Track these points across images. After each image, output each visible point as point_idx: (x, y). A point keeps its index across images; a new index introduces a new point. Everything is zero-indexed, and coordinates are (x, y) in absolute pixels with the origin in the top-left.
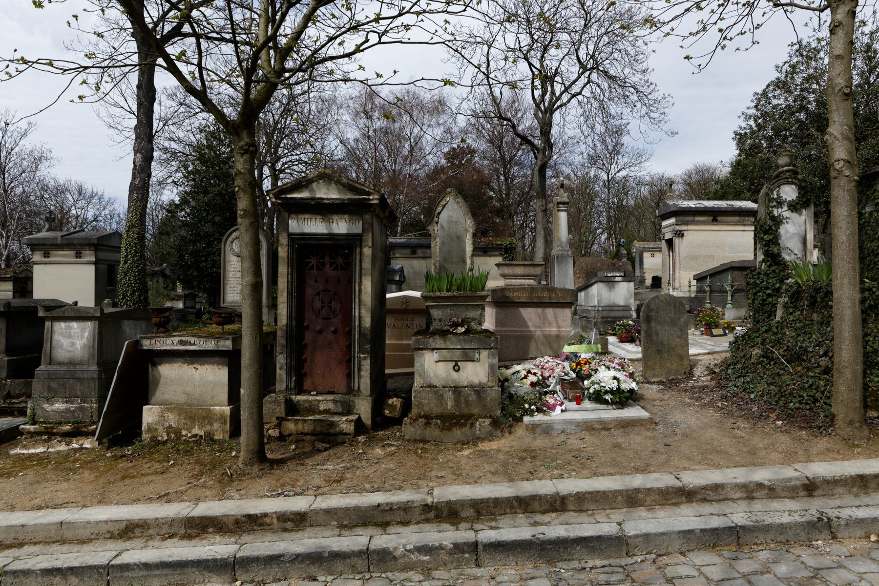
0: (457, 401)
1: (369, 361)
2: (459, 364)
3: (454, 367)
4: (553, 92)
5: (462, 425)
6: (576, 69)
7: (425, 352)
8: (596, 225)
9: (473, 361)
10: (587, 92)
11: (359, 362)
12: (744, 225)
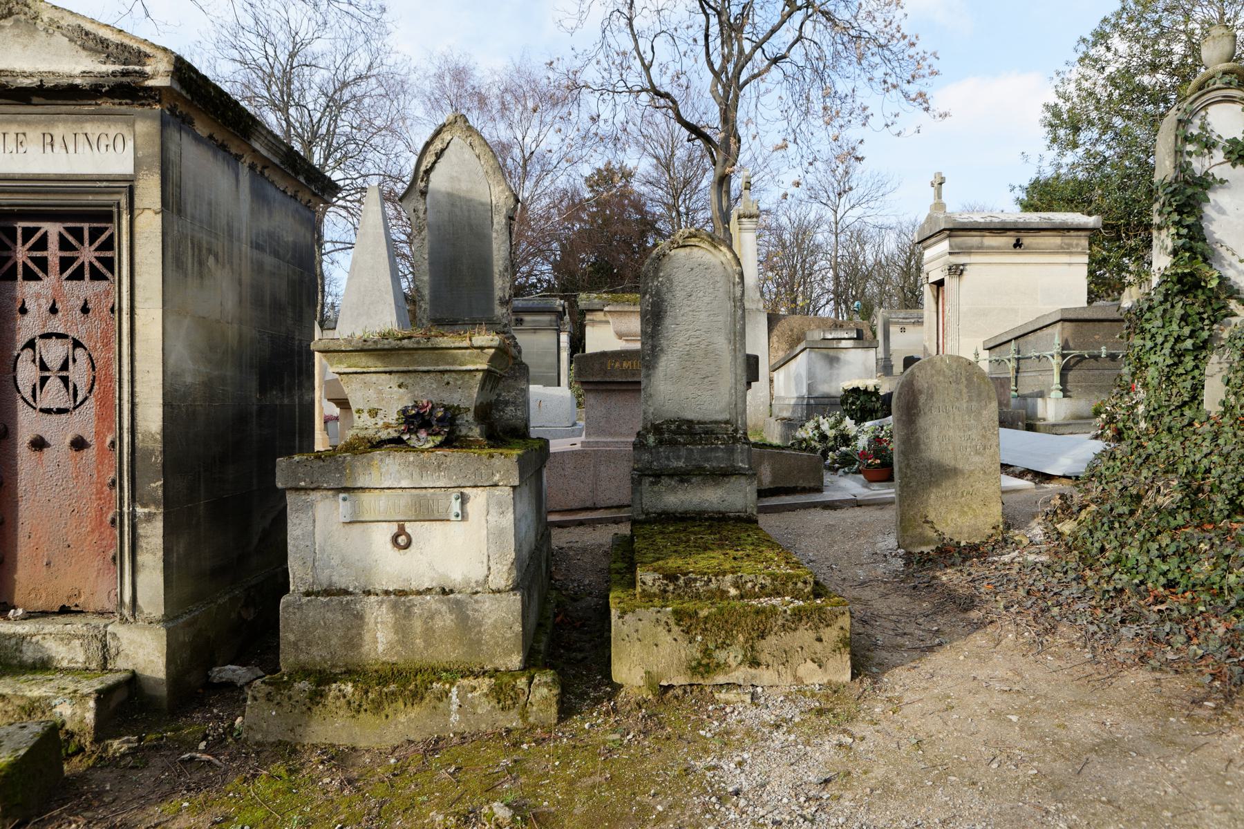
0: (403, 631)
2: (409, 528)
3: (395, 539)
4: (741, 51)
5: (417, 697)
8: (818, 291)
10: (797, 54)
12: (1071, 253)
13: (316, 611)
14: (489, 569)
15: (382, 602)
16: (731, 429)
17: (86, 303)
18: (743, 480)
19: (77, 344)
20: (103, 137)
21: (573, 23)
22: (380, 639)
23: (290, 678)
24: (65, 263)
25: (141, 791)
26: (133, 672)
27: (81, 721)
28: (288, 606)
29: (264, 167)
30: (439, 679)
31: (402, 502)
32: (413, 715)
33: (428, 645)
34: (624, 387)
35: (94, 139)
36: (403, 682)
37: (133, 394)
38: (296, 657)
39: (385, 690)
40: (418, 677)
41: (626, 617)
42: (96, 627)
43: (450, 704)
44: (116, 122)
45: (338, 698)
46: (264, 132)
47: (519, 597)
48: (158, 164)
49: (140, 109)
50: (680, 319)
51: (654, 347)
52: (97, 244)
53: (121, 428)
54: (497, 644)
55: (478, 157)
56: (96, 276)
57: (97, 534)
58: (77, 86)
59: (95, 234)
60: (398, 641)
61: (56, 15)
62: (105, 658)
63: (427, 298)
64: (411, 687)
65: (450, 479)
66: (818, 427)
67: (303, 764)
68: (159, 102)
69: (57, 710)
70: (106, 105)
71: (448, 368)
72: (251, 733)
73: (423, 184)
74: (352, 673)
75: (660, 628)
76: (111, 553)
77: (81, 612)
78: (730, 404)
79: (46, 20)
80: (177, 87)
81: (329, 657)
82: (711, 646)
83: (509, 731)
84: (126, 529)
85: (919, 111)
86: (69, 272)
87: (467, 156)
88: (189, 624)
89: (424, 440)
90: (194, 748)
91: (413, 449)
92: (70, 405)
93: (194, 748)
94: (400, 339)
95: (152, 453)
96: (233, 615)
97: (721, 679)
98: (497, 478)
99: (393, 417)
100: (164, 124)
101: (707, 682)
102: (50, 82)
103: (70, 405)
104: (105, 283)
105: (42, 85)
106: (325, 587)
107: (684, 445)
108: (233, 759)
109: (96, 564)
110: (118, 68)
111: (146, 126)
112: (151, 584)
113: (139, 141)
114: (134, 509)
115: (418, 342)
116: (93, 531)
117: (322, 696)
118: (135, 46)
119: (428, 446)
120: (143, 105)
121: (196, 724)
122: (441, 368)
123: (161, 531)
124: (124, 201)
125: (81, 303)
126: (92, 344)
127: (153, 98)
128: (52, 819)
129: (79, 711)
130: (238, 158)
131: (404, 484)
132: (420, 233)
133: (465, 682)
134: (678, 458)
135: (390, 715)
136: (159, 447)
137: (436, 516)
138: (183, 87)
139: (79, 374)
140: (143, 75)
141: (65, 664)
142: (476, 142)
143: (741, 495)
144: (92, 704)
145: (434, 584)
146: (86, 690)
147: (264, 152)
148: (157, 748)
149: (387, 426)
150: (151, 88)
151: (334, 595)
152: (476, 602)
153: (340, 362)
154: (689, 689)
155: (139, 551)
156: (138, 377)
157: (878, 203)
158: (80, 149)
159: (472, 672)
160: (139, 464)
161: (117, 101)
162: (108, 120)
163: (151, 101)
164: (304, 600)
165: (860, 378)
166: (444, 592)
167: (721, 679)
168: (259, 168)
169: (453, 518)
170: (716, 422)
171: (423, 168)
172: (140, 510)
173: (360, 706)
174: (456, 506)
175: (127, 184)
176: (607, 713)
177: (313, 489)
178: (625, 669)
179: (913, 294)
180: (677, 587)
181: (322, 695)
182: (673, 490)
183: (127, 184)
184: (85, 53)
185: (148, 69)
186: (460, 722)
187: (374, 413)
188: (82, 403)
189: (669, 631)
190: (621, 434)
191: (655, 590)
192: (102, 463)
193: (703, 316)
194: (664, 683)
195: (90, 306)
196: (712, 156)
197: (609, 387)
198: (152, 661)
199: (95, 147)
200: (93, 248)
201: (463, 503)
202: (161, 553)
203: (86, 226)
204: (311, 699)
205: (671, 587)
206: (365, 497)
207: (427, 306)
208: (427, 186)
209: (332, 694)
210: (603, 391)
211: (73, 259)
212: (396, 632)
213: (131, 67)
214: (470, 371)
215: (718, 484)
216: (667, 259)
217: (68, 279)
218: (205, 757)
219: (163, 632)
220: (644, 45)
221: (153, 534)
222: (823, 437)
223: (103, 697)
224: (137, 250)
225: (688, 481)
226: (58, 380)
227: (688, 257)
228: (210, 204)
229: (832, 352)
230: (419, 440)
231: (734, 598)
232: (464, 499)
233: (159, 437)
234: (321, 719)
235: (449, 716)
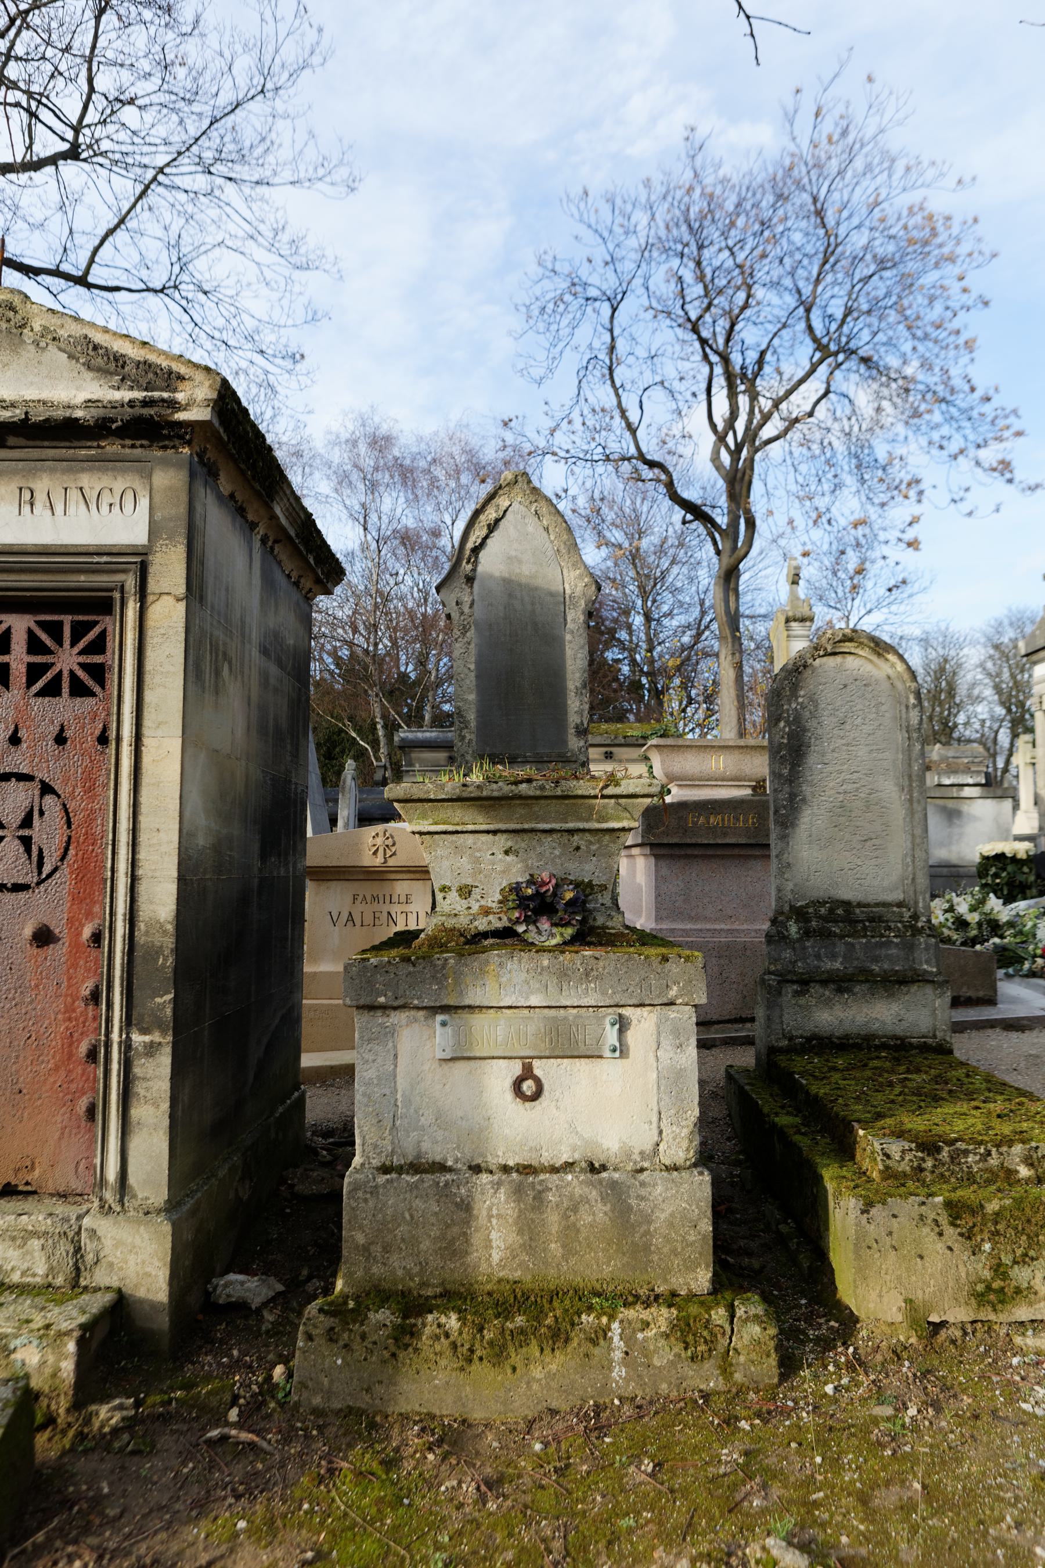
0: (529, 1229)
1: (165, 1061)
2: (539, 1068)
5: (558, 1337)
6: (806, 351)
7: (398, 1018)
9: (600, 1057)
11: (127, 1065)
13: (401, 1198)
14: (661, 1132)
15: (499, 1184)
16: (907, 915)
17: (62, 729)
18: (929, 990)
19: (47, 789)
20: (106, 492)
21: (541, 372)
22: (496, 1244)
23: (358, 1303)
24: (34, 672)
25: (156, 1497)
26: (119, 1291)
27: (54, 1375)
28: (356, 1187)
29: (276, 542)
30: (590, 1308)
31: (531, 1029)
32: (553, 1367)
33: (569, 1251)
34: (710, 852)
35: (92, 495)
36: (535, 1313)
37: (134, 864)
38: (367, 1270)
39: (509, 1325)
40: (556, 1304)
41: (874, 1211)
42: (66, 1220)
43: (610, 1349)
44: (124, 471)
45: (437, 1338)
46: (288, 492)
47: (707, 1177)
48: (183, 530)
49: (159, 453)
50: (829, 757)
51: (792, 796)
52: (81, 644)
53: (112, 914)
54: (674, 1252)
55: (547, 529)
56: (79, 690)
57: (63, 1073)
58: (77, 420)
59: (79, 631)
60: (523, 1246)
61: (53, 322)
62: (78, 1270)
63: (473, 725)
64: (549, 1321)
65: (604, 993)
66: (951, 909)
67: (397, 1450)
68: (189, 443)
69: (18, 1356)
70: (113, 447)
71: (581, 825)
72: (305, 1395)
73: (470, 567)
74: (456, 1296)
75: (926, 1230)
76: (83, 1104)
77: (34, 1193)
78: (903, 878)
79: (37, 328)
80: (216, 423)
81: (417, 1269)
82: (1007, 1259)
83: (706, 1396)
84: (115, 1066)
85: (998, 483)
86: (39, 684)
87: (530, 529)
88: (193, 1212)
89: (548, 934)
90: (220, 1420)
91: (527, 945)
92: (32, 878)
93: (220, 1420)
94: (516, 783)
95: (159, 951)
96: (232, 1196)
97: (1022, 1313)
98: (673, 992)
99: (493, 899)
100: (192, 475)
101: (1003, 1317)
102: (38, 415)
103: (32, 878)
104: (92, 701)
105: (27, 419)
106: (410, 1159)
107: (842, 937)
108: (287, 1440)
109: (59, 1119)
110: (139, 395)
111: (169, 477)
112: (150, 1152)
113: (157, 499)
114: (128, 1038)
115: (542, 788)
116: (57, 1068)
117: (412, 1334)
118: (164, 364)
119: (554, 942)
120: (165, 448)
121: (212, 1374)
122: (571, 825)
123: (168, 1070)
124: (130, 582)
125: (55, 729)
126: (69, 789)
127: (181, 437)
128: (38, 1551)
129: (51, 1359)
130: (253, 526)
131: (534, 1001)
132: (464, 634)
133: (631, 1313)
134: (833, 957)
135: (518, 1366)
136: (169, 942)
137: (582, 1050)
138: (222, 423)
139: (48, 833)
140: (173, 405)
141: (16, 1278)
142: (544, 510)
143: (926, 1012)
144: (71, 1347)
145: (577, 1156)
146: (65, 1326)
147: (283, 521)
148: (165, 1419)
149: (486, 912)
150: (180, 424)
151: (425, 1171)
152: (643, 1184)
153: (424, 817)
154: (969, 1329)
155: (134, 1102)
156: (143, 838)
157: (902, 608)
158: (72, 510)
159: (637, 1297)
160: (138, 969)
161: (129, 442)
162: (113, 469)
163: (177, 442)
164: (382, 1179)
165: (991, 840)
166: (592, 1169)
167: (1022, 1313)
168: (270, 543)
169: (607, 1054)
170: (884, 904)
171: (470, 545)
172: (137, 1038)
173: (472, 1351)
174: (611, 1036)
175: (138, 559)
176: (850, 1367)
177: (395, 1008)
178: (874, 1295)
179: (946, 725)
180: (940, 1163)
181: (414, 1333)
182: (828, 1003)
183: (138, 559)
184: (91, 374)
185: (180, 397)
186: (627, 1380)
187: (465, 892)
188: (49, 876)
189: (941, 1234)
190: (706, 919)
191: (905, 1167)
192: (75, 966)
193: (862, 752)
194: (935, 1318)
195: (68, 733)
196: (715, 543)
197: (689, 852)
198: (148, 1275)
199: (93, 507)
200: (76, 650)
201: (621, 1032)
202: (168, 1104)
203: (67, 620)
204: (396, 1339)
205: (929, 1164)
206: (479, 1022)
207: (473, 737)
208: (474, 570)
209: (428, 1330)
210: (680, 857)
211: (46, 667)
212: (520, 1232)
213: (156, 394)
214: (613, 830)
215: (891, 995)
216: (809, 671)
217: (38, 695)
218: (245, 1436)
219: (167, 1228)
220: (630, 402)
221: (156, 1075)
222: (961, 924)
223: (87, 1335)
224: (150, 654)
225: (849, 990)
226: (17, 842)
227: (840, 669)
228: (227, 590)
229: (950, 804)
230: (539, 932)
231: (1028, 1181)
232: (623, 1025)
233: (170, 928)
234: (412, 1373)
235: (610, 1369)
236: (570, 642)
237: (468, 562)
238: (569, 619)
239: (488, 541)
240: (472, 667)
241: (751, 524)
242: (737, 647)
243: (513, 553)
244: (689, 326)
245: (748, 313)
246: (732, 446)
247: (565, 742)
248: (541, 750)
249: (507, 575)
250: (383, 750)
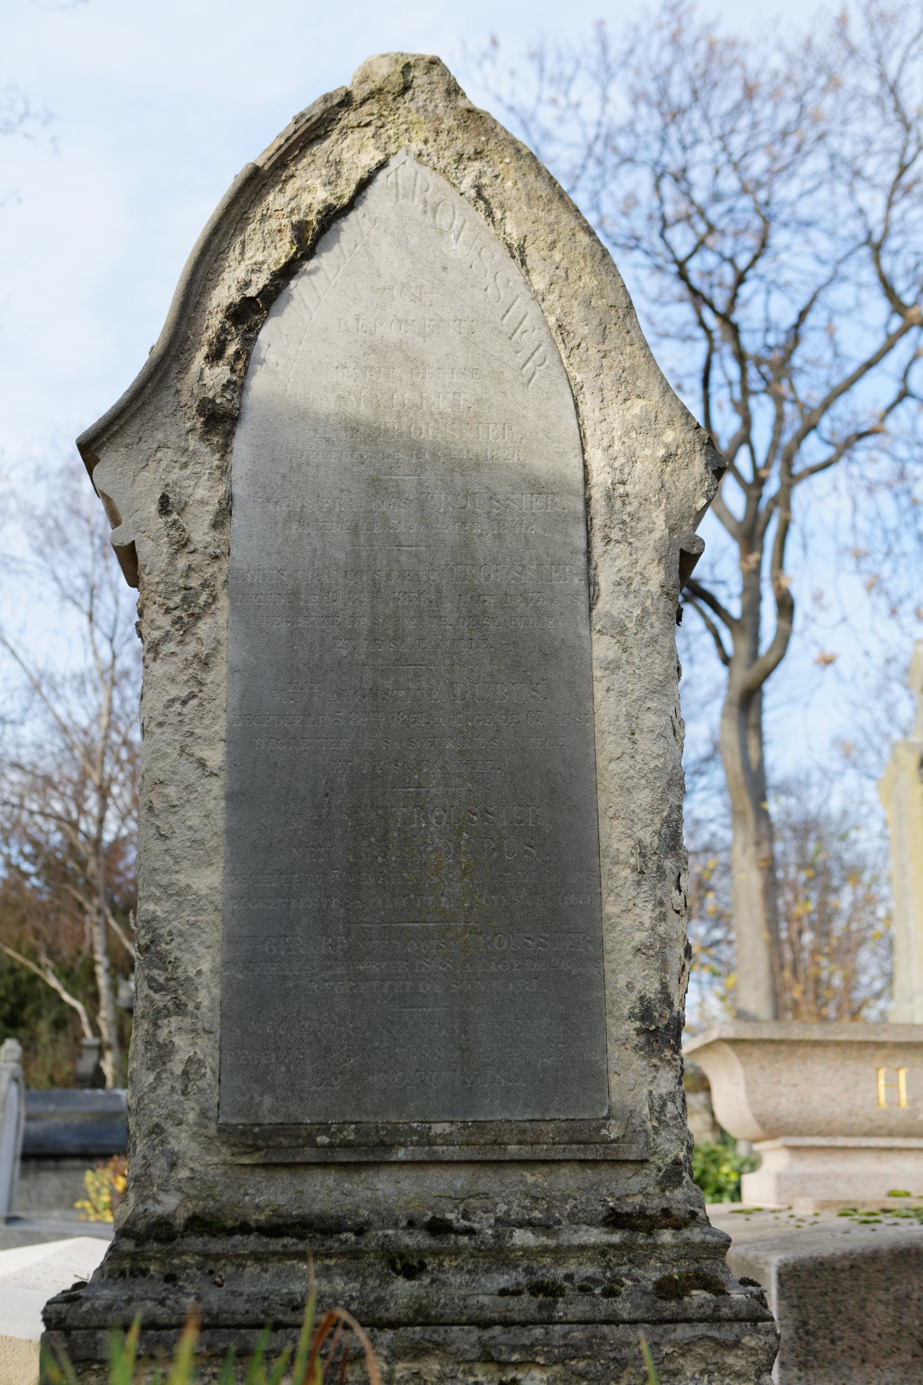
55: (518, 253)
63: (207, 996)
73: (220, 373)
87: (456, 249)
142: (509, 186)
171: (224, 294)
207: (205, 1049)
208: (237, 386)
236: (613, 667)
237: (215, 356)
238: (605, 578)
239: (297, 286)
240: (215, 756)
241: (786, 606)
242: (764, 829)
243: (392, 334)
244: (674, 268)
245: (763, 265)
246: (748, 475)
247: (594, 1078)
248: (493, 1112)
249: (363, 411)
250: (105, 1015)
